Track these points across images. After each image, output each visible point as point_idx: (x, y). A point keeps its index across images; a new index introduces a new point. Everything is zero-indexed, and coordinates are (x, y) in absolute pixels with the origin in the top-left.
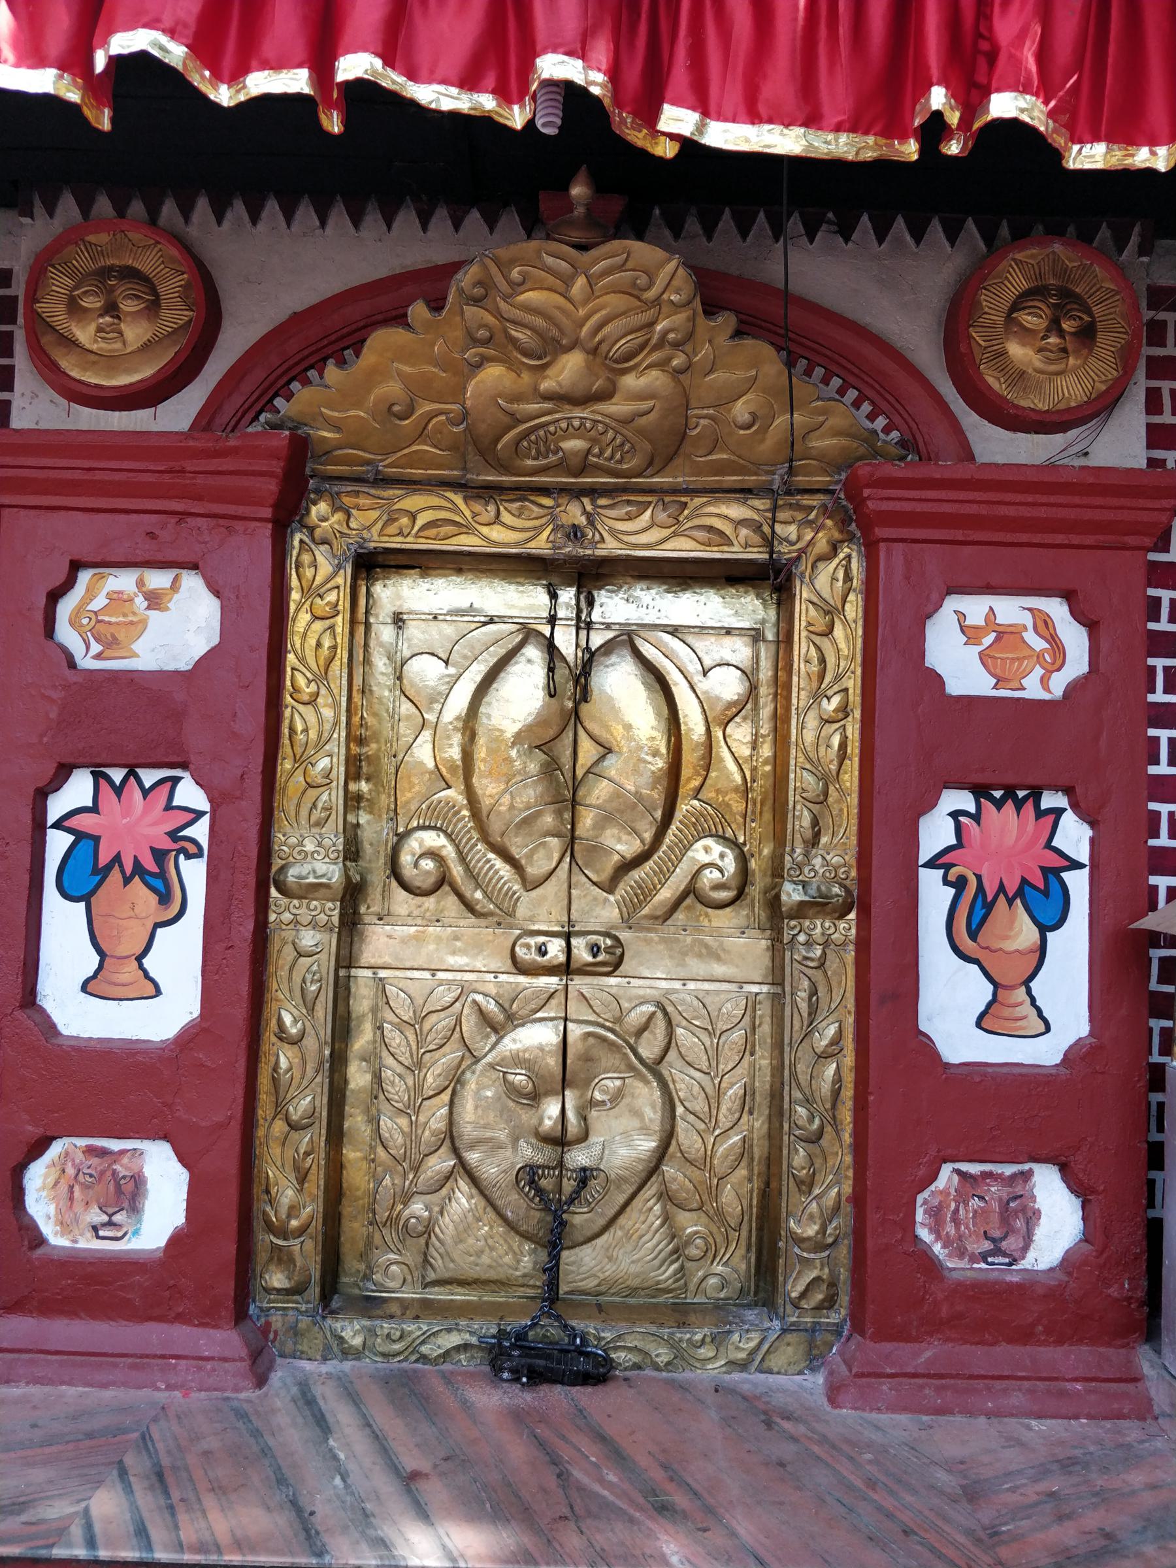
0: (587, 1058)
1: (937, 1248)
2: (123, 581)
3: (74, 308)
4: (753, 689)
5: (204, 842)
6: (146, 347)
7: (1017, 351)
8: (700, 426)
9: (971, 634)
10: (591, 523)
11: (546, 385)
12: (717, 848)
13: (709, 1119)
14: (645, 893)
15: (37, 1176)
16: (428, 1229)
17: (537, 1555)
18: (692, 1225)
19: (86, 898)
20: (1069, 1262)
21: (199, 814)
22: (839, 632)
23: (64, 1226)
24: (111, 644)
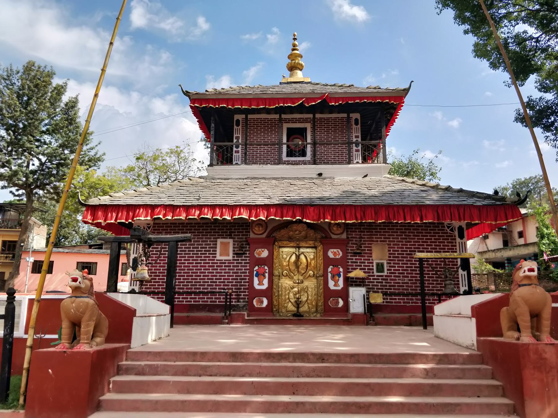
0: (301, 291)
2: (260, 250)
5: (76, 349)
7: (334, 229)
8: (308, 235)
9: (332, 252)
13: (312, 296)
14: (305, 276)
16: (287, 307)
18: (310, 306)
20: (342, 306)
23: (257, 305)
24: (259, 255)
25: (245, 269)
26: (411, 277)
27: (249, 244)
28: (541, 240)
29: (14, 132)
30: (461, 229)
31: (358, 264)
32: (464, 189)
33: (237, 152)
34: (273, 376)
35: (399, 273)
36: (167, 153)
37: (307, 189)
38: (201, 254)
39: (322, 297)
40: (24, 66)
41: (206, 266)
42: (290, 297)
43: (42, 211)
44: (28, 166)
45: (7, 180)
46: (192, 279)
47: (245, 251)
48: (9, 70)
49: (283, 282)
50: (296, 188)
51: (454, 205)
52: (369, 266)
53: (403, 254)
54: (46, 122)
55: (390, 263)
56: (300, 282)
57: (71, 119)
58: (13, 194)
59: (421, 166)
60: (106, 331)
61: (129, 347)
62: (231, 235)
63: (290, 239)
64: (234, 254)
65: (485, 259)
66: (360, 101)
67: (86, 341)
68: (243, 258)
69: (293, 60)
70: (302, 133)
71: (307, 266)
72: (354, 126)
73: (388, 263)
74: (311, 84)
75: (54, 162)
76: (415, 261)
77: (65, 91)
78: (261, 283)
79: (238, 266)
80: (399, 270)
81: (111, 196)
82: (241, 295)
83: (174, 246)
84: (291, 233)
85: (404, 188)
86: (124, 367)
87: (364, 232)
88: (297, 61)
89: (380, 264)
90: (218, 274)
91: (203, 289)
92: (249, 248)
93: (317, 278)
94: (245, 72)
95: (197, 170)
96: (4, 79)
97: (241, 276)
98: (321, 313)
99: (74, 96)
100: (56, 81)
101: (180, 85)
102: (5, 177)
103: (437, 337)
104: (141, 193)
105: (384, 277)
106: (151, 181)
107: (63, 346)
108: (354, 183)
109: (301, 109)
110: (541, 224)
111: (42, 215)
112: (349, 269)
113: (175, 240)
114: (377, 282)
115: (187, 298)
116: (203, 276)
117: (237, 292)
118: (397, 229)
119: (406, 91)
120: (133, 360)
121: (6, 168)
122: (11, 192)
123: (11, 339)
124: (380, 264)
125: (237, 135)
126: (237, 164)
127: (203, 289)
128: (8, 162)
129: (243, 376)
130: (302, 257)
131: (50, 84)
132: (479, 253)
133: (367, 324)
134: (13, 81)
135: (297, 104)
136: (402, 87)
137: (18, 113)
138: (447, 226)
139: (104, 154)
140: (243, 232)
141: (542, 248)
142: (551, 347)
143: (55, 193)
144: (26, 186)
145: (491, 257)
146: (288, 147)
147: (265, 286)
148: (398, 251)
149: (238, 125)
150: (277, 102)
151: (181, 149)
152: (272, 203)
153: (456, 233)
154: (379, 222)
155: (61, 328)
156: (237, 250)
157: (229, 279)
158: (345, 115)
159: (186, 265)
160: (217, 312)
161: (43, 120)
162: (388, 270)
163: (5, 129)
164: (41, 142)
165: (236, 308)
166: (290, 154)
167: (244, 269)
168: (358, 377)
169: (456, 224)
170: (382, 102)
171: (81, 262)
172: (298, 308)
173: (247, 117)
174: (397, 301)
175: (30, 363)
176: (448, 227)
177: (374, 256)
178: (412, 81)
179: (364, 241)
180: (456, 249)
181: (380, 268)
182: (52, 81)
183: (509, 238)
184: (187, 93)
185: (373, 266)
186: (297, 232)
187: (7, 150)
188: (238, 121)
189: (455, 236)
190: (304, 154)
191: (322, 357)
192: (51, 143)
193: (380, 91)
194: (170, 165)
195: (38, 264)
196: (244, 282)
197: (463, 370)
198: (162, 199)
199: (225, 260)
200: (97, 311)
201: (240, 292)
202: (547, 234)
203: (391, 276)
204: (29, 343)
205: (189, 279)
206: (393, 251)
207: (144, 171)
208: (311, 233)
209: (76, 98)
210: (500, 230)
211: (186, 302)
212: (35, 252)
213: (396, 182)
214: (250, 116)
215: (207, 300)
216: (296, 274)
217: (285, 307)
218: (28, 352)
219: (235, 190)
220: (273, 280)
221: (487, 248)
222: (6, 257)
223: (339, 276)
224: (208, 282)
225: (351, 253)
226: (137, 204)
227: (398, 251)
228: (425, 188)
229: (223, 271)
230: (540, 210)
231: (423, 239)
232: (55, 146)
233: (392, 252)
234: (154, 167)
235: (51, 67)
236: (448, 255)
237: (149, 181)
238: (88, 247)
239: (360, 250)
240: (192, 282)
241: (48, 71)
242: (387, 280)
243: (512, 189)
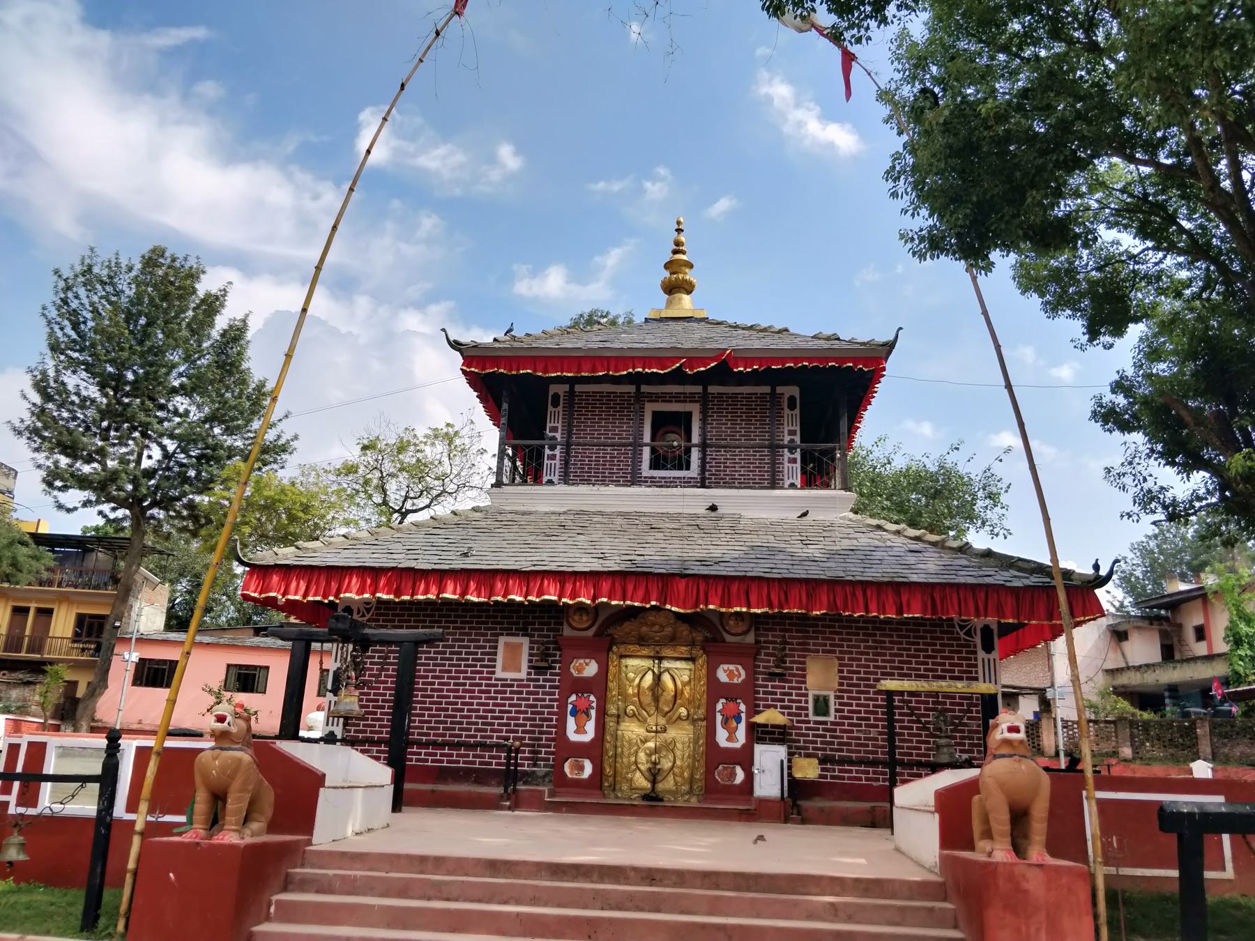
2: (581, 661)
9: (725, 671)
14: (671, 718)
16: (632, 779)
18: (678, 779)
20: (742, 783)
23: (571, 773)
24: (580, 671)
27: (560, 650)
28: (1234, 647)
29: (116, 390)
30: (987, 631)
31: (778, 696)
32: (995, 550)
33: (553, 457)
34: (559, 906)
35: (858, 719)
36: (426, 436)
37: (682, 538)
38: (466, 666)
39: (703, 762)
40: (143, 257)
41: (473, 691)
42: (639, 761)
43: (161, 553)
44: (139, 461)
45: (94, 490)
46: (445, 716)
47: (554, 662)
48: (113, 264)
50: (660, 535)
51: (965, 585)
52: (800, 701)
54: (182, 369)
57: (231, 364)
58: (105, 516)
59: (966, 479)
60: (269, 812)
61: (309, 843)
62: (527, 630)
63: (642, 641)
64: (530, 667)
65: (1113, 687)
67: (233, 827)
68: (548, 677)
69: (674, 273)
71: (675, 696)
73: (837, 697)
74: (708, 323)
75: (192, 454)
77: (222, 306)
78: (580, 730)
79: (537, 693)
82: (540, 752)
83: (410, 653)
84: (644, 629)
85: (877, 543)
86: (298, 877)
87: (791, 631)
89: (821, 699)
90: (497, 708)
91: (467, 736)
92: (560, 656)
93: (694, 722)
94: (597, 259)
95: (488, 472)
96: (103, 283)
99: (240, 316)
100: (205, 286)
101: (443, 330)
102: (92, 482)
103: (898, 850)
104: (355, 542)
105: (829, 726)
106: (392, 495)
107: (194, 834)
109: (678, 377)
111: (160, 559)
112: (758, 706)
113: (413, 639)
114: (814, 736)
115: (435, 755)
117: (533, 746)
119: (890, 346)
120: (313, 866)
121: (95, 465)
122: (100, 513)
123: (108, 819)
124: (821, 699)
125: (552, 424)
126: (550, 482)
127: (467, 736)
128: (102, 452)
129: (505, 903)
130: (666, 678)
131: (194, 291)
132: (1107, 671)
133: (786, 820)
134: (120, 287)
135: (669, 370)
137: (125, 354)
139: (296, 438)
141: (1236, 667)
142: (1037, 870)
143: (191, 517)
144: (134, 503)
145: (1133, 683)
146: (653, 451)
147: (589, 734)
148: (859, 672)
149: (555, 404)
150: (631, 365)
151: (456, 429)
152: (606, 569)
153: (978, 640)
154: (814, 613)
155: (194, 803)
156: (536, 661)
157: (518, 719)
158: (767, 389)
159: (436, 686)
160: (492, 786)
161: (174, 366)
162: (837, 710)
163: (98, 384)
164: (169, 411)
165: (528, 777)
166: (655, 465)
167: (549, 699)
168: (710, 914)
169: (978, 622)
170: (839, 367)
171: (236, 665)
172: (654, 782)
175: (139, 860)
176: (962, 628)
177: (810, 680)
178: (901, 328)
179: (790, 650)
180: (976, 672)
182: (197, 286)
183: (1175, 640)
184: (456, 345)
185: (807, 702)
186: (657, 628)
187: (99, 427)
188: (556, 396)
189: (975, 646)
190: (684, 464)
191: (651, 875)
192: (187, 412)
193: (836, 344)
194: (432, 463)
195: (147, 666)
196: (548, 726)
197: (902, 909)
198: (395, 556)
199: (511, 680)
200: (256, 775)
202: (1247, 635)
204: (139, 827)
206: (849, 672)
207: (378, 474)
208: (684, 630)
210: (1155, 622)
212: (143, 641)
213: (864, 530)
214: (578, 388)
215: (473, 760)
217: (627, 780)
218: (136, 840)
219: (539, 538)
220: (604, 724)
221: (1127, 663)
222: (83, 650)
223: (739, 720)
226: (346, 564)
227: (859, 672)
228: (919, 546)
229: (507, 702)
230: (1232, 582)
232: (195, 418)
233: (845, 674)
234: (398, 466)
237: (386, 495)
238: (252, 632)
240: (446, 722)
241: (191, 268)
242: (835, 731)
243: (1196, 527)
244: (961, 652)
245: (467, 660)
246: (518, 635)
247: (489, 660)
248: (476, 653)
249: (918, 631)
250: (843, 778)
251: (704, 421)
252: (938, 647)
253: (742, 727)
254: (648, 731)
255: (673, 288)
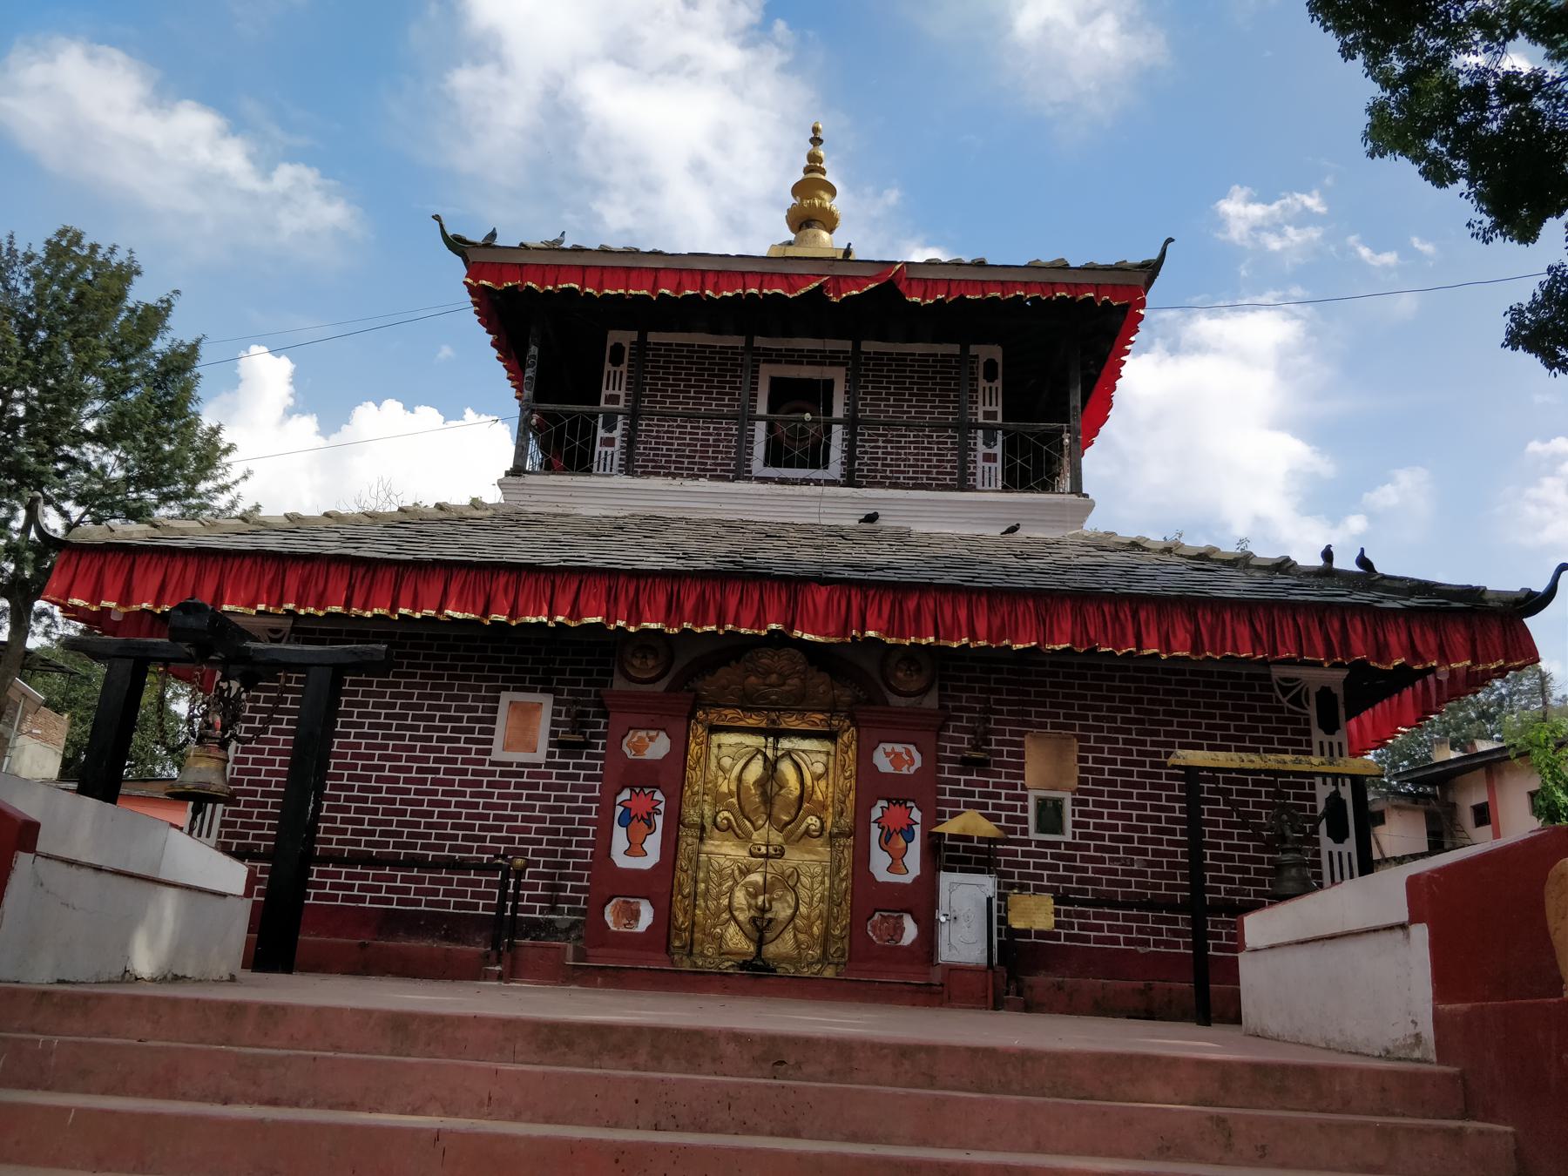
0: (772, 884)
1: (874, 938)
2: (642, 734)
3: (633, 655)
4: (827, 769)
6: (653, 667)
7: (900, 675)
9: (887, 754)
10: (778, 718)
11: (768, 682)
12: (814, 818)
13: (810, 904)
14: (792, 833)
15: (608, 909)
16: (721, 937)
17: (810, 175)
18: (801, 937)
19: (627, 827)
21: (661, 802)
22: (850, 753)
23: (616, 924)
24: (638, 751)
25: (585, 800)
26: (1156, 853)
27: (606, 715)
30: (1325, 696)
33: (609, 442)
34: (548, 1120)
35: (1112, 838)
39: (846, 907)
42: (736, 905)
47: (593, 735)
49: (713, 849)
51: (1306, 604)
52: (1014, 808)
53: (1130, 774)
54: (98, 405)
55: (1086, 803)
56: (771, 850)
63: (748, 703)
64: (551, 744)
66: (1003, 295)
68: (584, 761)
70: (819, 394)
71: (801, 798)
72: (982, 383)
73: (1075, 802)
76: (1169, 776)
78: (635, 849)
80: (1116, 828)
81: (155, 526)
82: (564, 888)
87: (998, 692)
88: (817, 202)
92: (606, 726)
97: (572, 821)
98: (837, 964)
99: (188, 342)
100: (140, 293)
101: (437, 218)
108: (971, 543)
110: (1549, 776)
114: (1037, 866)
116: (441, 815)
118: (1110, 689)
119: (1151, 270)
124: (1050, 804)
125: (610, 392)
130: (786, 768)
133: (997, 1005)
136: (1136, 258)
138: (1280, 686)
140: (590, 673)
146: (771, 429)
153: (1312, 712)
158: (955, 349)
159: (386, 773)
162: (1076, 824)
170: (1073, 299)
172: (760, 943)
173: (642, 337)
174: (1106, 933)
176: (1285, 691)
178: (1170, 240)
179: (997, 722)
181: (1050, 815)
184: (457, 244)
185: (1025, 809)
189: (1307, 722)
196: (579, 844)
199: (520, 765)
201: (562, 877)
203: (1087, 848)
205: (390, 823)
208: (821, 684)
209: (194, 349)
211: (373, 900)
216: (760, 822)
217: (714, 937)
223: (909, 838)
224: (455, 837)
225: (950, 760)
227: (1114, 762)
231: (1199, 726)
235: (131, 252)
236: (1288, 761)
239: (982, 751)
240: (400, 834)
241: (120, 265)
242: (1073, 858)
244: (1284, 731)
245: (444, 729)
246: (534, 690)
247: (481, 731)
248: (460, 719)
249: (1213, 696)
250: (1086, 939)
251: (851, 395)
252: (1246, 723)
253: (915, 848)
254: (752, 855)
255: (806, 218)
